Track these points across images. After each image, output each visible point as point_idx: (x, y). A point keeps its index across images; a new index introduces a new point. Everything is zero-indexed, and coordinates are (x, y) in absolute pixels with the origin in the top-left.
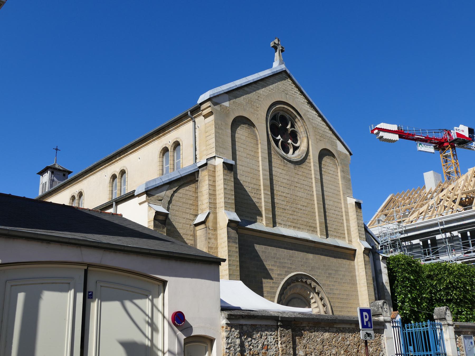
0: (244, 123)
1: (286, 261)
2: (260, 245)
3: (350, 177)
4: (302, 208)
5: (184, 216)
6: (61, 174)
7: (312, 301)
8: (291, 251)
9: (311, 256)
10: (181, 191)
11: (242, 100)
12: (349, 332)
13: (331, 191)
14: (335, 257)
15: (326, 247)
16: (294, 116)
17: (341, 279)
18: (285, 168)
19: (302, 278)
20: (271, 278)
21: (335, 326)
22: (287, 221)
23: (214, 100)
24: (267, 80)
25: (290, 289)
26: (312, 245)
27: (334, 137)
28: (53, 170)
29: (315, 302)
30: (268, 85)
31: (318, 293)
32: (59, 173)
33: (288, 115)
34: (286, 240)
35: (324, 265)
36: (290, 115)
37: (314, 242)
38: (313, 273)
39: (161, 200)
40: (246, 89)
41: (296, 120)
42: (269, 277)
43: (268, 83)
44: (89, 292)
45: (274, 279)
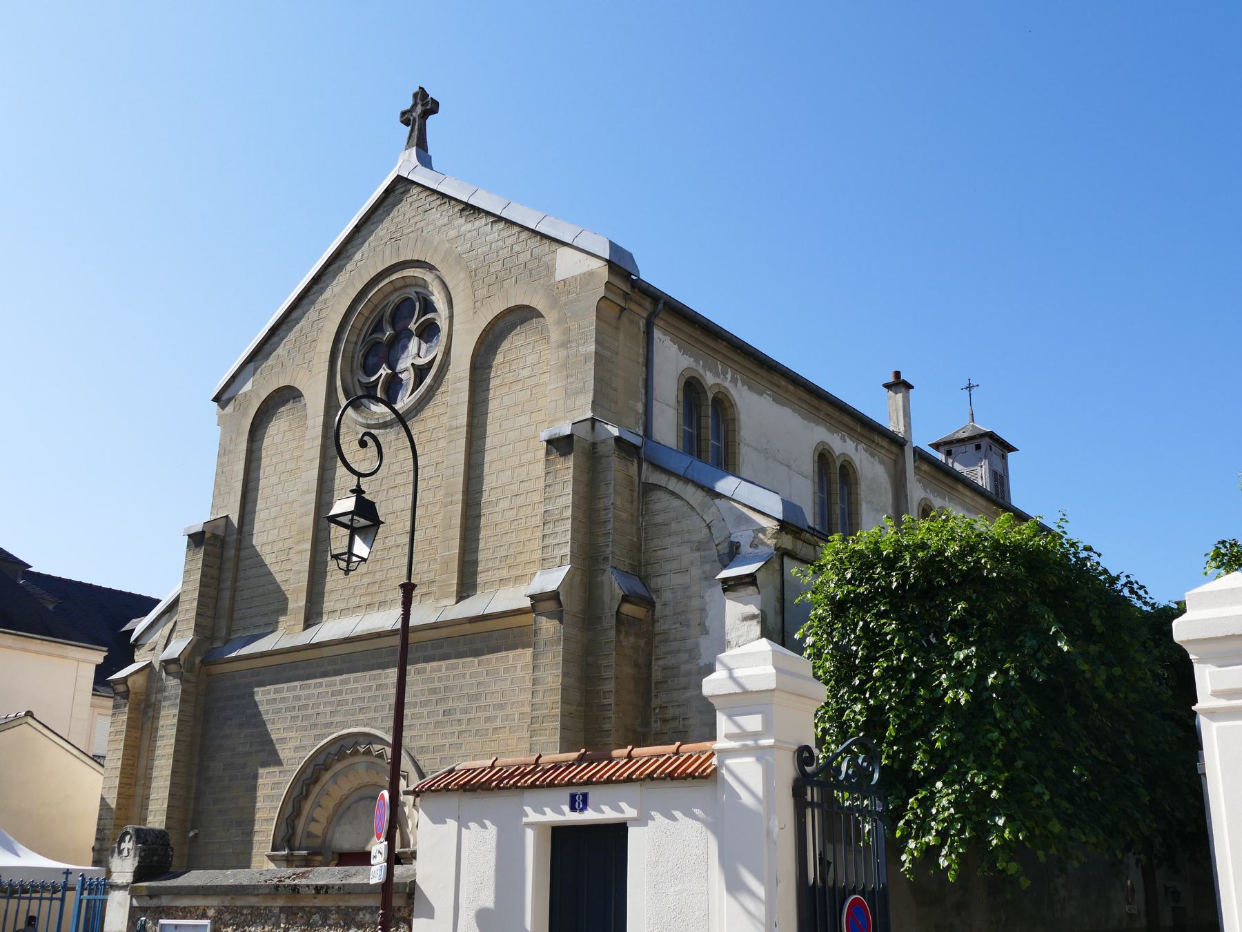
1: (321, 709)
6: (971, 447)
14: (476, 653)
15: (443, 633)
19: (357, 743)
23: (225, 397)
28: (947, 448)
32: (962, 449)
34: (326, 652)
36: (396, 290)
40: (295, 315)
42: (273, 759)
44: (585, 796)
45: (285, 763)
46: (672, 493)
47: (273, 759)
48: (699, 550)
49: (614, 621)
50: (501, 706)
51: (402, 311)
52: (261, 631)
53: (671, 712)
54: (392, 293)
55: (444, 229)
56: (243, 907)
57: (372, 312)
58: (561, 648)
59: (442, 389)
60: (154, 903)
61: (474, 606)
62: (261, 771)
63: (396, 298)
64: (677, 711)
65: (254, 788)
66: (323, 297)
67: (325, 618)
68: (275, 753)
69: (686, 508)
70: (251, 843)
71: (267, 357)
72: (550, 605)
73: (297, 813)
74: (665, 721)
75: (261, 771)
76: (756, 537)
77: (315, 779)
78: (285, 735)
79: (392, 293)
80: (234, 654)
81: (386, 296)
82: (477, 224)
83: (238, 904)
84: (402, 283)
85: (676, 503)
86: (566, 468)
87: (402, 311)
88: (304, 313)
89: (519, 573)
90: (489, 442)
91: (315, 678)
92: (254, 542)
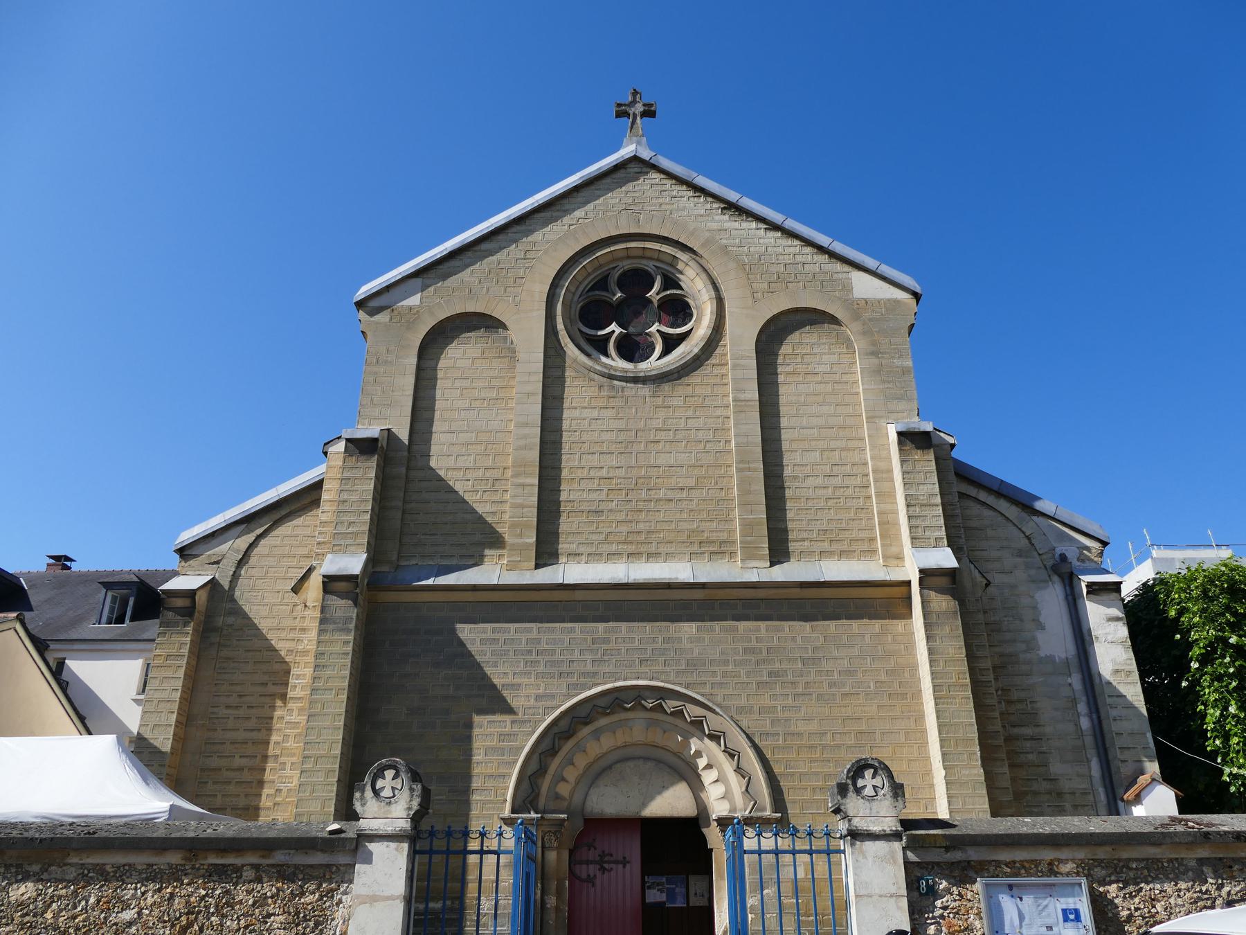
0: (799, 326)
2: (475, 622)
3: (910, 363)
4: (670, 495)
5: (278, 588)
7: (702, 763)
8: (601, 626)
9: (689, 629)
10: (281, 531)
11: (469, 276)
12: (144, 881)
13: (815, 421)
15: (761, 593)
16: (669, 260)
17: (832, 685)
18: (617, 402)
20: (509, 710)
21: (75, 860)
22: (606, 541)
23: (374, 303)
24: (566, 201)
25: (597, 734)
26: (698, 594)
27: (838, 266)
29: (709, 766)
30: (568, 212)
31: (715, 737)
33: (651, 263)
35: (751, 650)
37: (703, 585)
38: (694, 678)
39: (217, 563)
40: (485, 246)
41: (680, 266)
42: (497, 703)
43: (567, 207)
46: (984, 504)
47: (497, 703)
48: (1020, 556)
49: (317, 614)
50: (850, 672)
51: (637, 280)
52: (454, 562)
53: (1015, 695)
54: (622, 259)
55: (700, 219)
56: (1129, 860)
57: (595, 270)
58: (351, 637)
59: (712, 361)
60: (957, 856)
61: (780, 574)
62: (477, 719)
63: (627, 265)
64: (1023, 695)
65: (468, 739)
66: (530, 239)
67: (563, 559)
68: (503, 700)
69: (1000, 518)
70: (467, 804)
71: (445, 277)
72: (944, 582)
73: (542, 770)
74: (1010, 702)
75: (477, 719)
76: (1082, 553)
77: (568, 734)
78: (517, 680)
79: (622, 259)
80: (430, 582)
81: (614, 260)
82: (745, 225)
83: (1125, 855)
84: (640, 253)
85: (987, 513)
86: (369, 469)
87: (637, 280)
88: (501, 249)
89: (845, 547)
90: (784, 422)
91: (563, 621)
92: (433, 463)
